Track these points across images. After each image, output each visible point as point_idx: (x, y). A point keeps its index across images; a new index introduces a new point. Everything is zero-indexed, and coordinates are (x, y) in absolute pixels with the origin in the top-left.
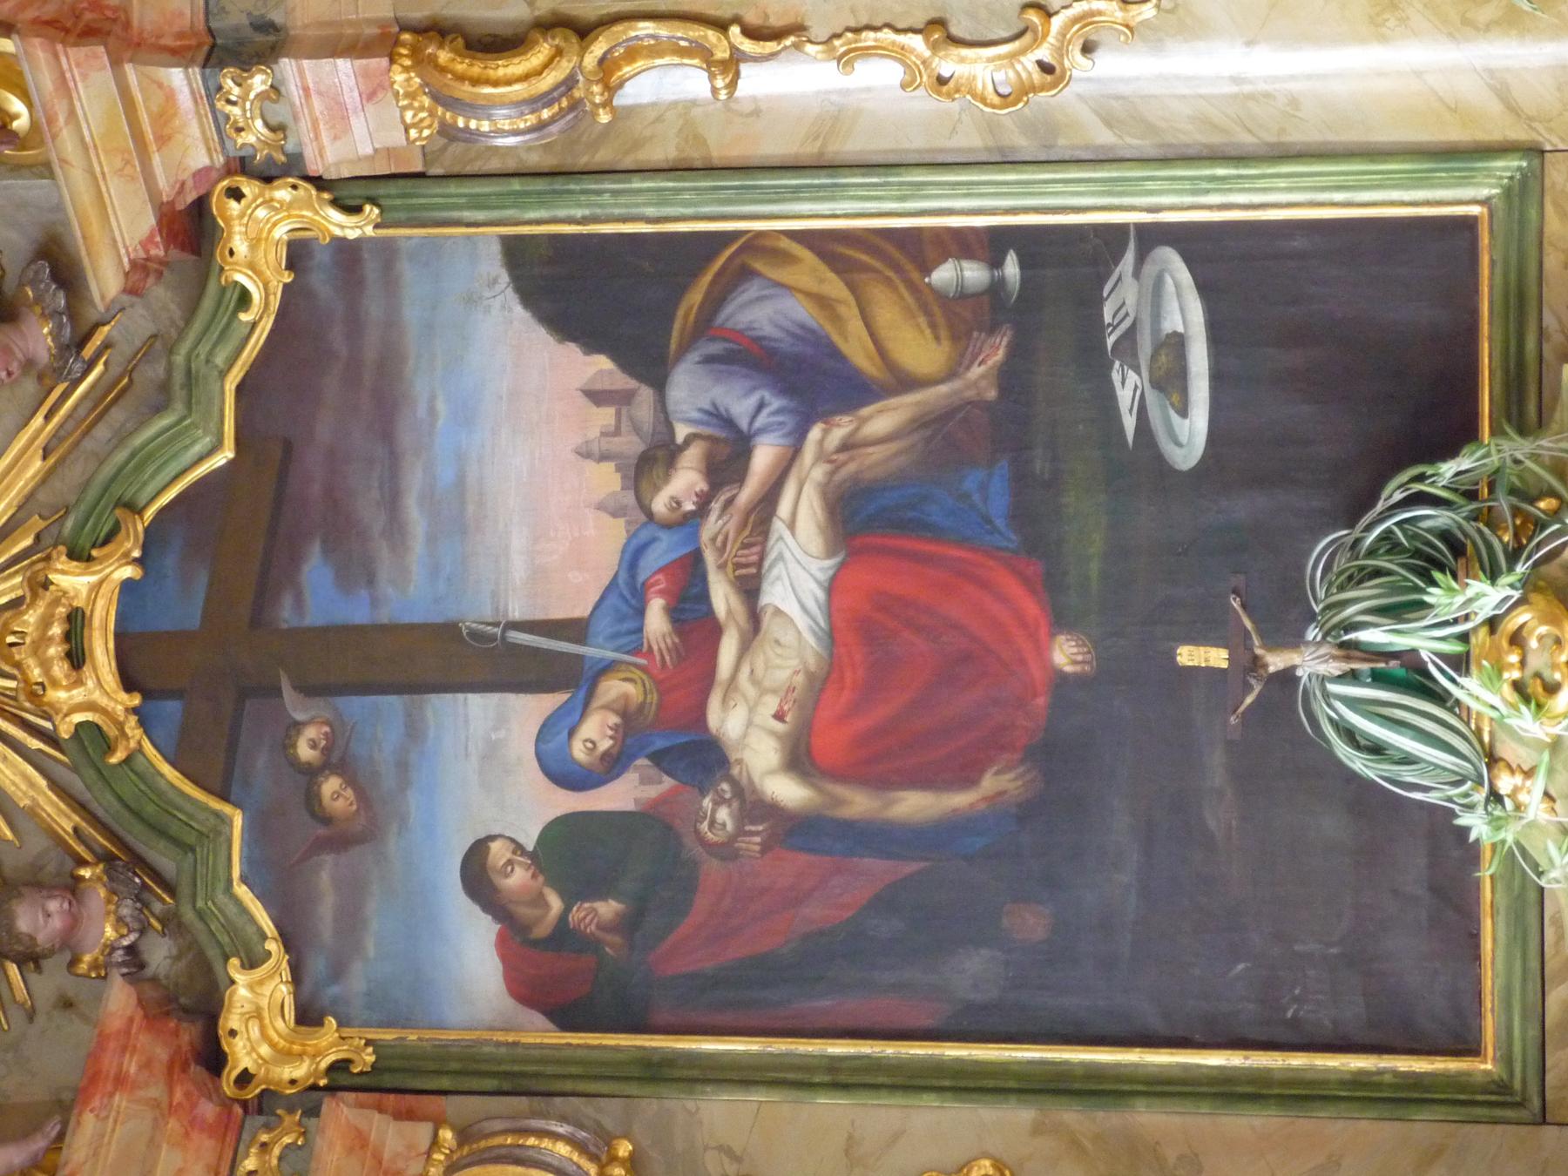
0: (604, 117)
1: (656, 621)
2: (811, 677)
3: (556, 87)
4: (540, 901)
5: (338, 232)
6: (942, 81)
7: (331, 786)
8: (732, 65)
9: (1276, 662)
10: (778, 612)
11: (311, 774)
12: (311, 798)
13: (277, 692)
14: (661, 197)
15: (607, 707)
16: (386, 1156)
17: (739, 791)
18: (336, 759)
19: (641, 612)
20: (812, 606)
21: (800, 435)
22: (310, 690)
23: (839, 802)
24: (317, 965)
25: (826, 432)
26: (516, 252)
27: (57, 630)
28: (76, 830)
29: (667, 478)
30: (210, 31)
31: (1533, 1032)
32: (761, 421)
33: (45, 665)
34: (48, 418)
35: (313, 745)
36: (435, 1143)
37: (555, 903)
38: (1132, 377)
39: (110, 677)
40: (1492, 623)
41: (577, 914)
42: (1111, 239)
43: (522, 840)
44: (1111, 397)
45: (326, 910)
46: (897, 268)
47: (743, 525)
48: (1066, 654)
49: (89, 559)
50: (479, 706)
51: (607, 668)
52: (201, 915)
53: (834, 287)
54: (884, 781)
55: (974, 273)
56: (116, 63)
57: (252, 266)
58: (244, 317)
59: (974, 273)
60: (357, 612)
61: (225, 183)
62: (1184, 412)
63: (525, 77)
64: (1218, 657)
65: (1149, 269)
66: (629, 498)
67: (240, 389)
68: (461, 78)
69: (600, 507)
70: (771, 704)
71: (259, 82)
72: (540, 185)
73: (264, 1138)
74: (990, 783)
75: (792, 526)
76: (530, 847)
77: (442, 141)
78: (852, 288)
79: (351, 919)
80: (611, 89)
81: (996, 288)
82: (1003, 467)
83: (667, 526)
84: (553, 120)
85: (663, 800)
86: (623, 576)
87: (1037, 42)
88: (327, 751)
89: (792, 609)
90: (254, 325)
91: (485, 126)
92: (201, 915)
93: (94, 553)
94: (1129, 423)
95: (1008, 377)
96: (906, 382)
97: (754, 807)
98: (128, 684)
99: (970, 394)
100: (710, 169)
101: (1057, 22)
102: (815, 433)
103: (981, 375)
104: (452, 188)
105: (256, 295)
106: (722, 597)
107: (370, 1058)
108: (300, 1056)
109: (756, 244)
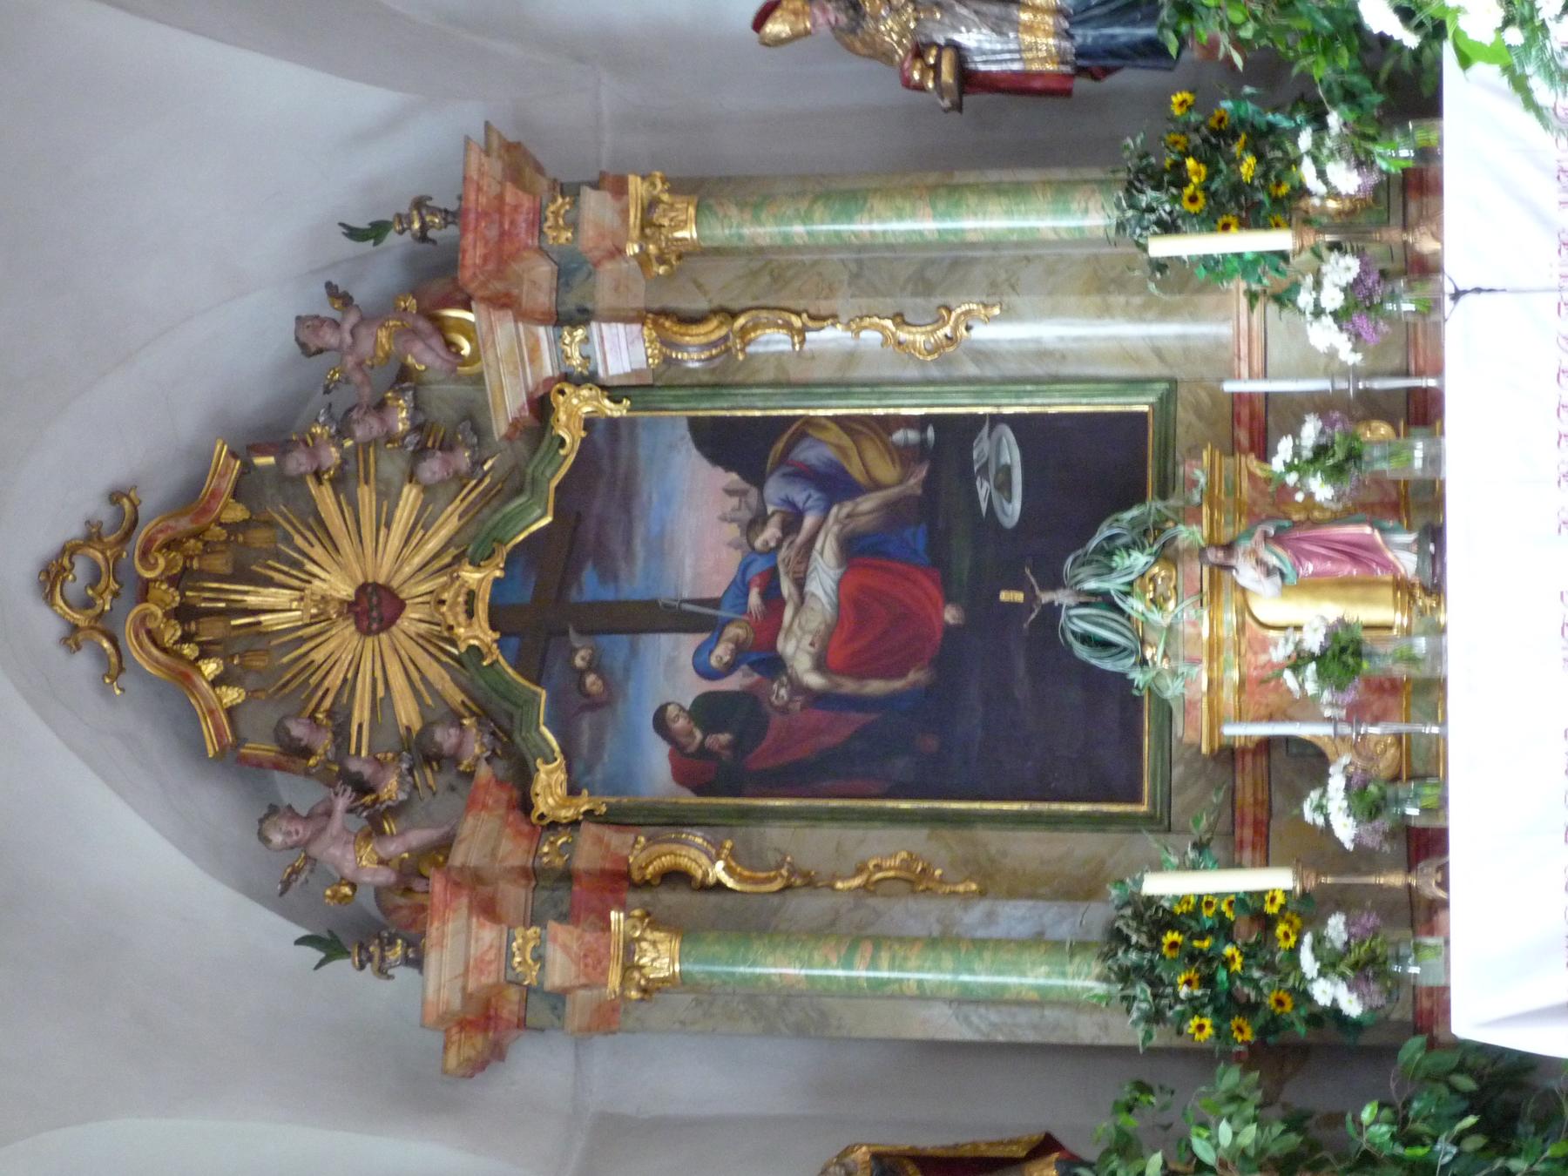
0: (741, 357)
1: (754, 599)
2: (828, 626)
3: (720, 339)
4: (691, 734)
5: (609, 413)
6: (900, 343)
7: (591, 679)
8: (802, 331)
9: (1046, 597)
10: (813, 595)
11: (582, 673)
12: (581, 684)
13: (566, 633)
14: (766, 397)
15: (729, 640)
16: (612, 847)
17: (790, 679)
18: (594, 666)
19: (747, 595)
20: (829, 591)
21: (827, 510)
22: (582, 632)
23: (839, 686)
24: (579, 767)
25: (839, 510)
26: (695, 425)
27: (461, 599)
28: (463, 702)
29: (762, 531)
30: (558, 313)
31: (1166, 789)
32: (810, 503)
33: (456, 616)
34: (462, 500)
35: (583, 659)
36: (636, 841)
37: (698, 735)
38: (986, 484)
39: (486, 625)
40: (1142, 575)
41: (710, 740)
42: (975, 422)
43: (683, 704)
44: (976, 493)
45: (585, 738)
46: (875, 432)
47: (797, 555)
48: (951, 615)
49: (479, 566)
50: (665, 640)
51: (730, 621)
52: (524, 739)
53: (846, 441)
54: (862, 675)
55: (913, 436)
56: (516, 321)
57: (567, 427)
58: (562, 452)
59: (913, 436)
60: (608, 594)
61: (558, 386)
62: (1010, 500)
63: (706, 334)
64: (1019, 597)
65: (995, 435)
66: (744, 541)
67: (557, 488)
68: (676, 333)
69: (730, 544)
70: (808, 639)
71: (580, 333)
72: (708, 391)
73: (552, 839)
74: (912, 676)
75: (822, 553)
76: (688, 708)
77: (664, 367)
78: (854, 442)
79: (597, 745)
80: (746, 344)
81: (923, 442)
82: (924, 526)
83: (762, 553)
84: (717, 356)
85: (751, 687)
86: (739, 577)
87: (945, 324)
88: (590, 663)
89: (820, 593)
90: (566, 457)
91: (686, 356)
92: (524, 739)
93: (482, 563)
94: (984, 506)
95: (927, 483)
96: (877, 486)
97: (798, 688)
98: (493, 627)
99: (909, 492)
100: (790, 384)
101: (954, 315)
102: (834, 510)
103: (914, 483)
104: (666, 392)
105: (568, 440)
106: (786, 587)
107: (604, 809)
108: (569, 807)
109: (809, 421)
